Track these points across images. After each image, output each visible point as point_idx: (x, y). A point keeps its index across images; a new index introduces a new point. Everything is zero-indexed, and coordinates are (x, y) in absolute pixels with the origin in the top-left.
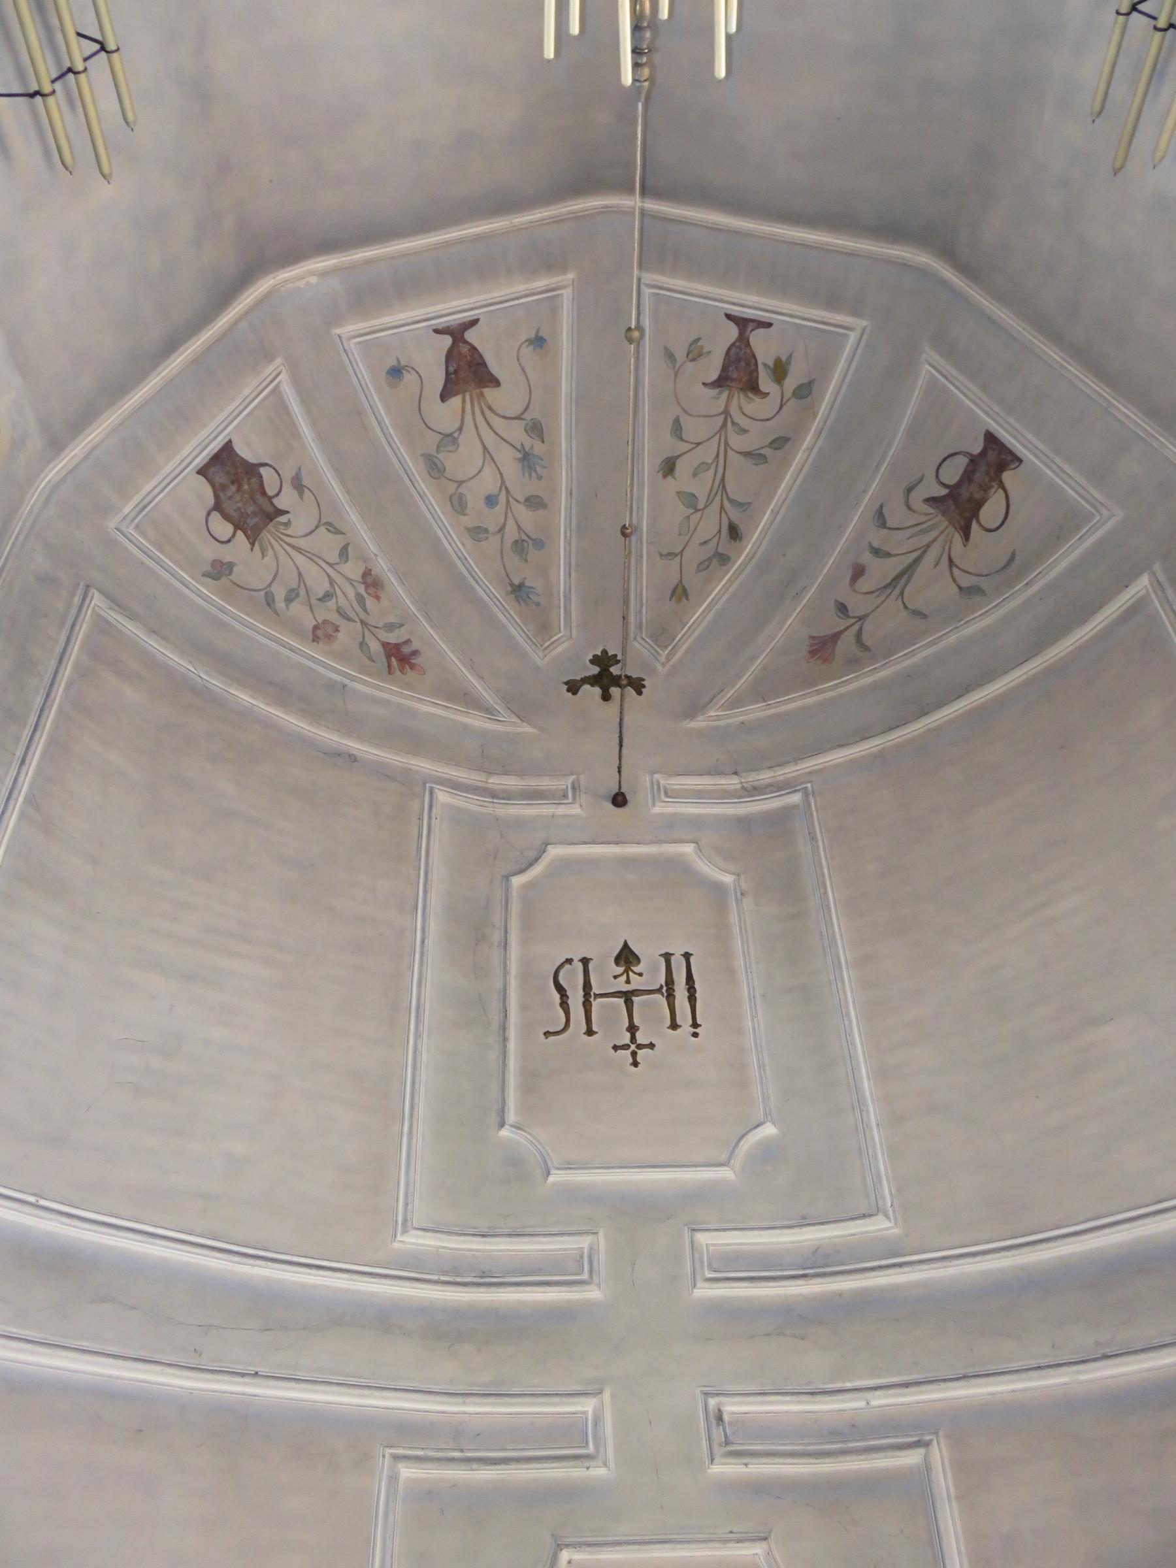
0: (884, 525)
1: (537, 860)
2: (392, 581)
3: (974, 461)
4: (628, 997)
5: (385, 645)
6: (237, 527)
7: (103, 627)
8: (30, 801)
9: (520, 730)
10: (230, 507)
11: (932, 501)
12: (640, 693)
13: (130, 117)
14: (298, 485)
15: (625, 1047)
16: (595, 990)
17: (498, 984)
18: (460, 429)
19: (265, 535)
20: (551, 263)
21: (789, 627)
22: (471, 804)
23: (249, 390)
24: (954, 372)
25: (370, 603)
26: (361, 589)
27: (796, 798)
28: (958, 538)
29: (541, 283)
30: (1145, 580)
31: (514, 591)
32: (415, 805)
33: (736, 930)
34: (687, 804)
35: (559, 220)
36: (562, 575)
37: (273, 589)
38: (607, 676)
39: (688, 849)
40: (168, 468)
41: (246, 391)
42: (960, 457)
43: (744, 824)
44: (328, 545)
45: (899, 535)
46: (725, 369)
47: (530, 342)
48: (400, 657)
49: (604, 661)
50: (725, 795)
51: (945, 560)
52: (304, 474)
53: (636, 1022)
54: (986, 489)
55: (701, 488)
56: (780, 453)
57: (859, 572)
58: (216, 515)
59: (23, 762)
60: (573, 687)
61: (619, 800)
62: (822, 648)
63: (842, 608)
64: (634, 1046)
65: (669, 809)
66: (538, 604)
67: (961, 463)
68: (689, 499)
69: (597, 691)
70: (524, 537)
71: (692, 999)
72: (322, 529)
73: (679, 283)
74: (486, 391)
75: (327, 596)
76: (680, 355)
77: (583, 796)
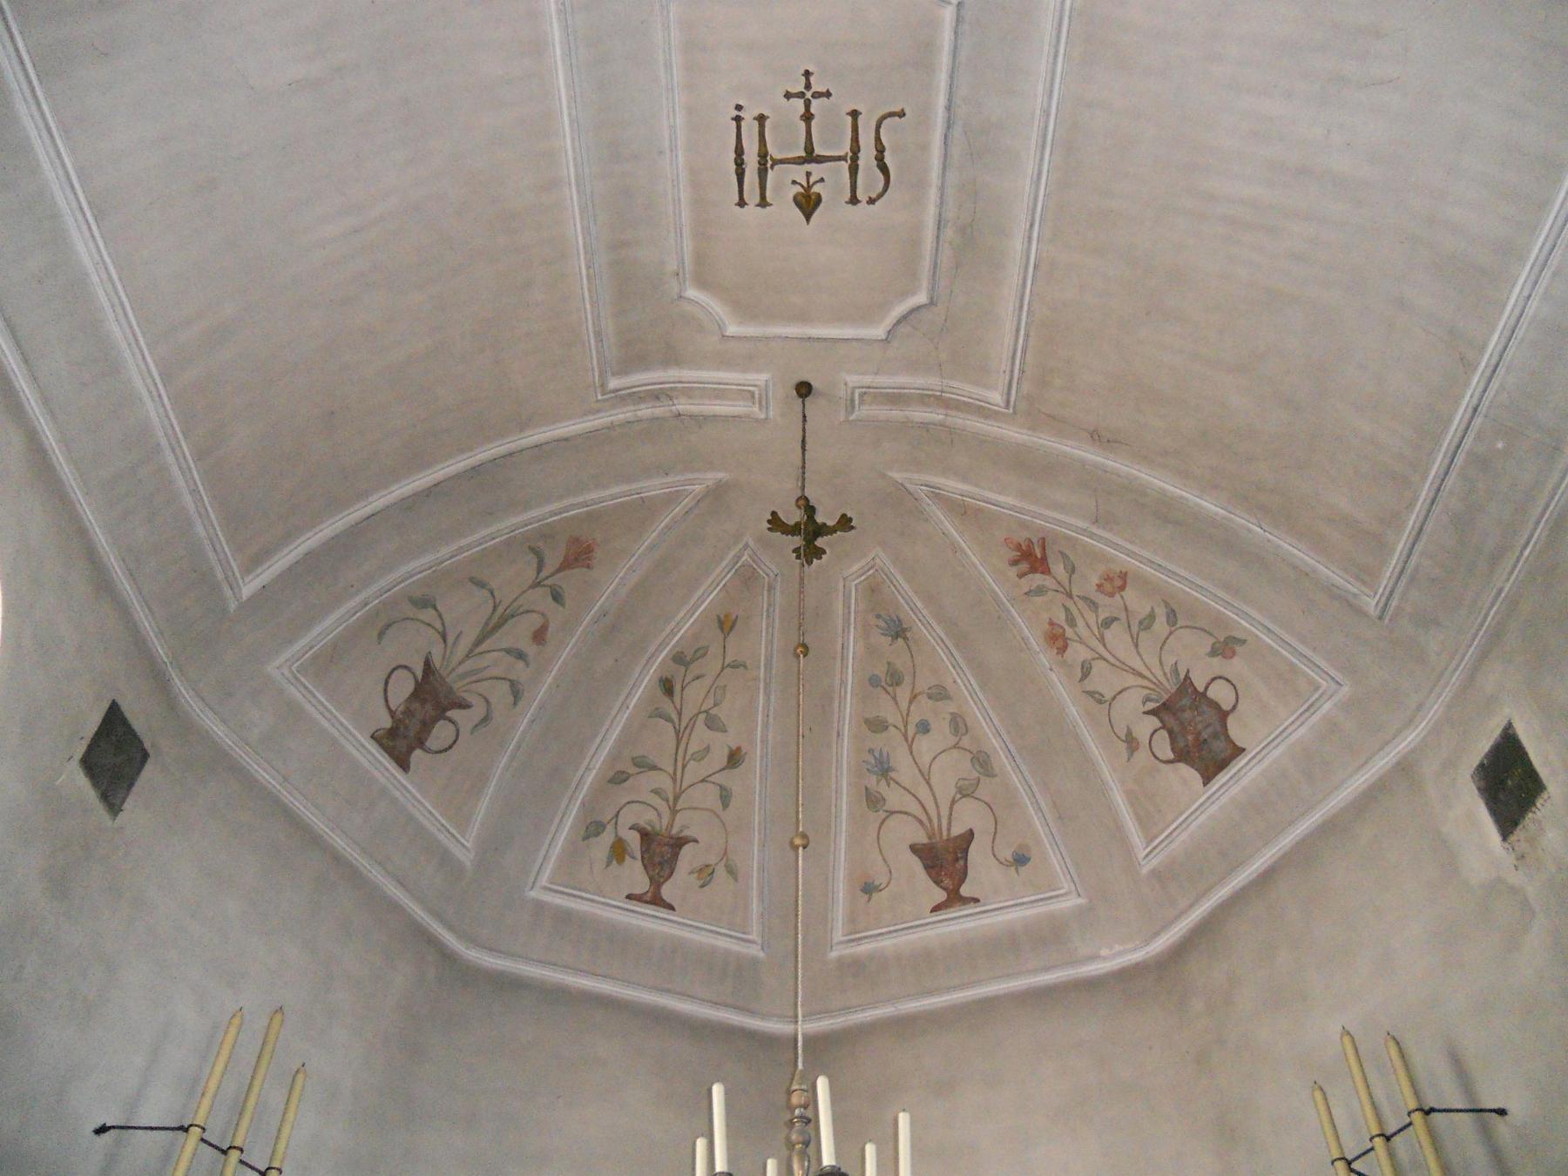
0: (513, 684)
1: (899, 322)
2: (1035, 642)
3: (420, 743)
4: (810, 157)
5: (1047, 571)
6: (1204, 695)
7: (1366, 575)
8: (1469, 367)
9: (905, 475)
10: (1210, 715)
11: (464, 705)
12: (774, 514)
13: (1318, 1095)
14: (1131, 742)
15: (817, 95)
16: (845, 166)
17: (952, 177)
18: (953, 802)
19: (1171, 687)
20: (855, 968)
21: (613, 581)
22: (965, 389)
23: (1179, 840)
24: (441, 837)
25: (1061, 618)
26: (1069, 632)
27: (613, 383)
28: (437, 662)
29: (864, 948)
30: (248, 589)
31: (904, 630)
32: (1026, 387)
33: (686, 232)
34: (731, 387)
35: (846, 1009)
36: (850, 649)
37: (1166, 629)
38: (809, 534)
39: (732, 329)
40: (1277, 753)
41: (1184, 836)
42: (434, 748)
43: (671, 358)
44: (1104, 680)
45: (495, 672)
46: (675, 856)
47: (878, 889)
48: (1031, 557)
49: (810, 552)
50: (688, 393)
51: (450, 640)
52: (1125, 755)
53: (803, 124)
54: (408, 712)
55: (701, 735)
56: (619, 767)
57: (539, 636)
58: (1226, 707)
59: (1475, 410)
60: (845, 523)
61: (804, 389)
62: (580, 555)
63: (557, 597)
64: (808, 95)
65: (751, 377)
66: (878, 616)
67: (433, 742)
68: (713, 724)
69: (819, 519)
70: (890, 689)
71: (739, 151)
72: (1108, 697)
73: (722, 943)
74: (925, 840)
75: (1107, 623)
76: (721, 871)
77: (842, 393)
